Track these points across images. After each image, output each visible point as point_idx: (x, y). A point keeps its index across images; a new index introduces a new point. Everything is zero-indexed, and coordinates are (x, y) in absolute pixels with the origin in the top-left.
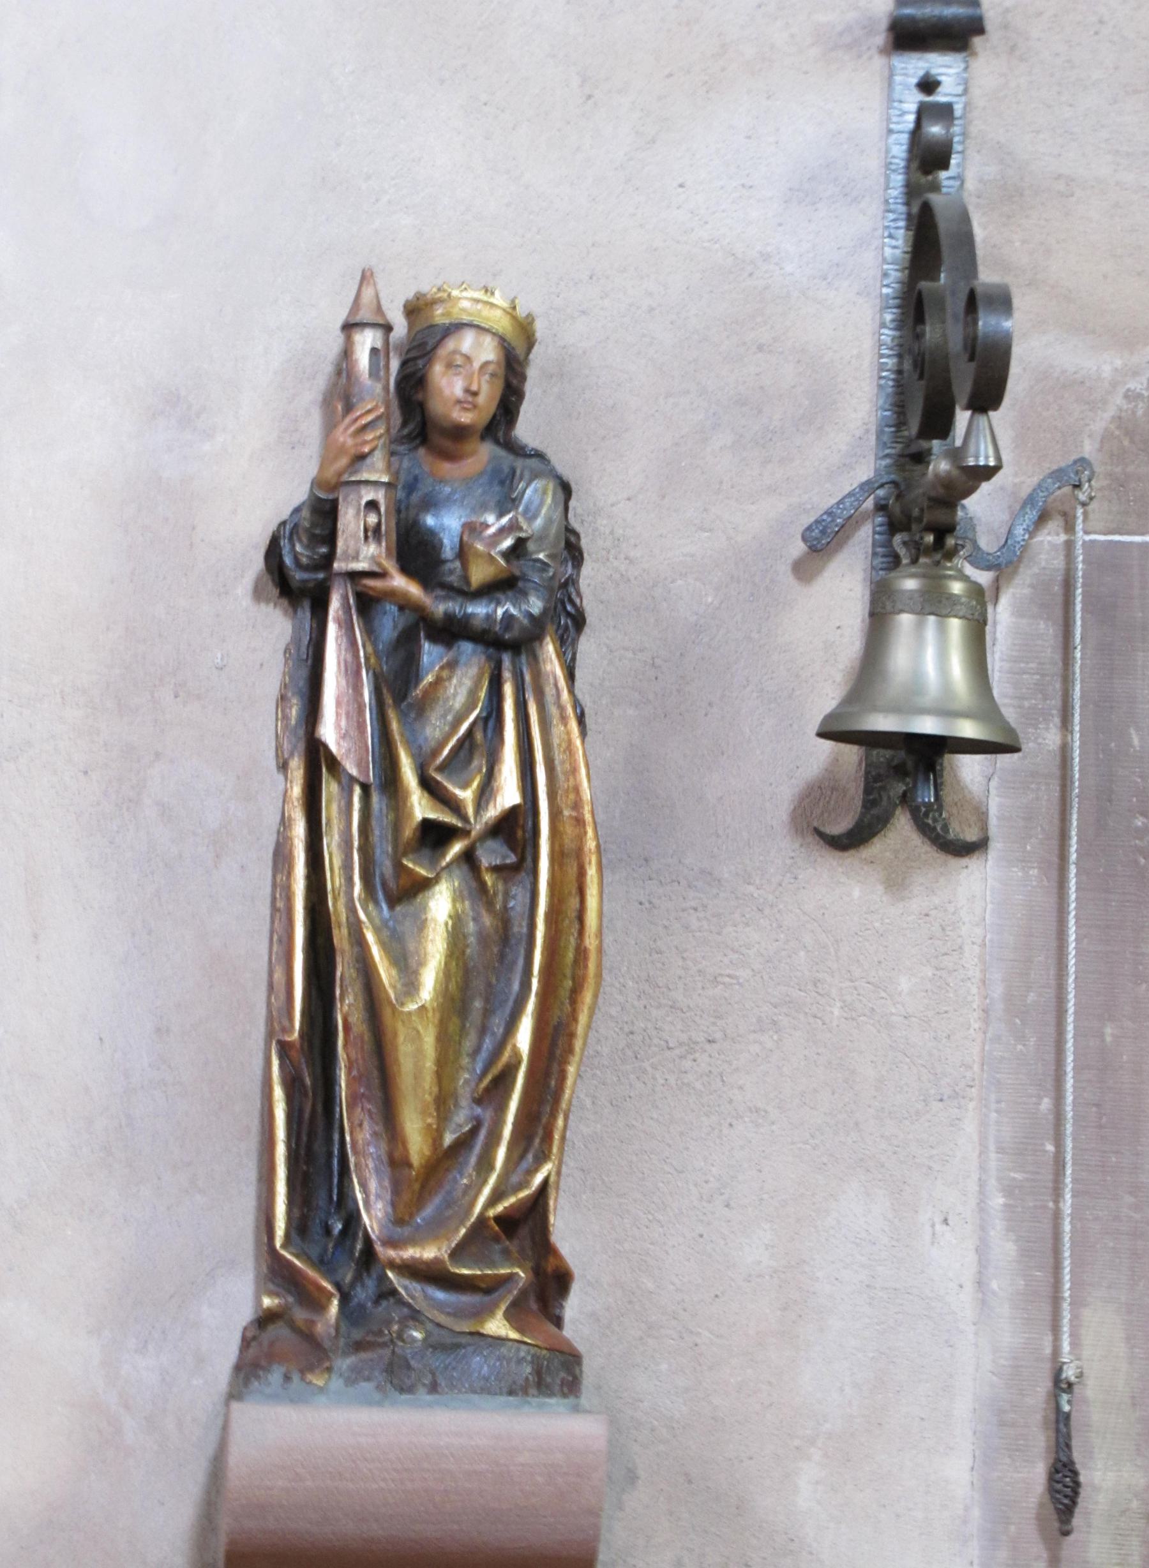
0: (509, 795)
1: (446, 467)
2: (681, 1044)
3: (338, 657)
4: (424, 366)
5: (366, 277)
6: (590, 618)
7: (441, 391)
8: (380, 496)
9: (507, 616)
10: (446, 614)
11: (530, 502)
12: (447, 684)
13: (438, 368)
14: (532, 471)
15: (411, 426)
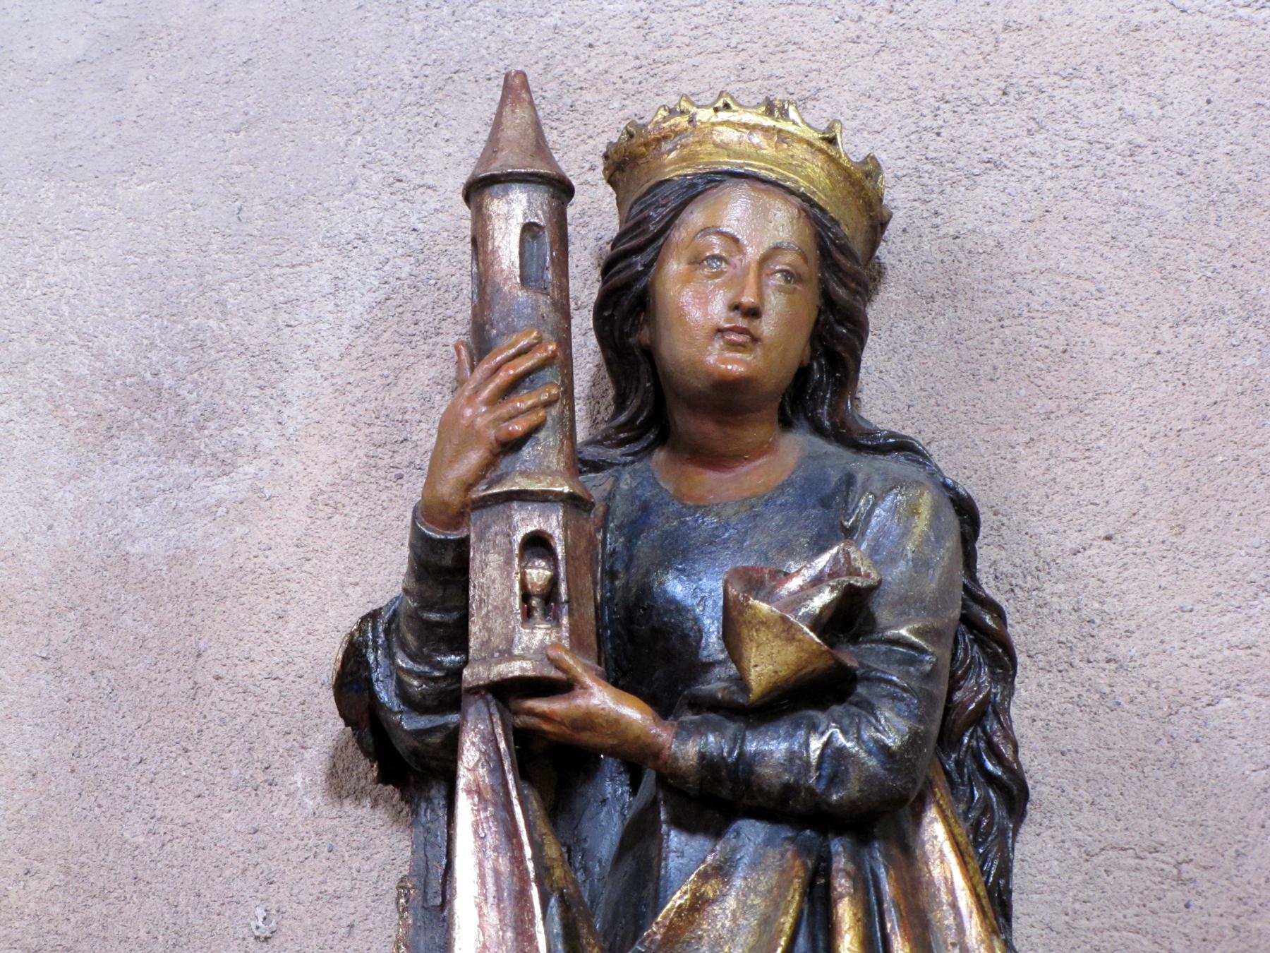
1: (709, 482)
3: (480, 864)
4: (648, 266)
5: (515, 88)
6: (1037, 791)
7: (682, 317)
8: (553, 523)
9: (833, 754)
10: (702, 756)
11: (883, 532)
12: (716, 909)
13: (674, 267)
14: (885, 476)
15: (633, 404)
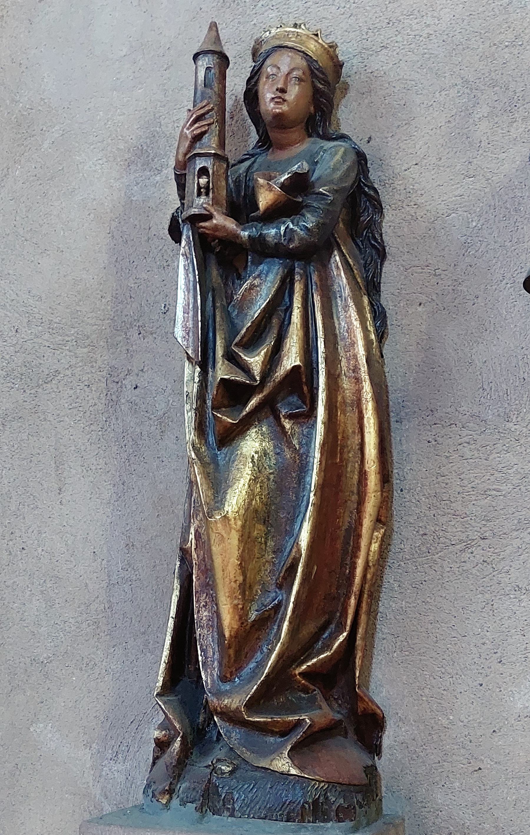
0: (292, 358)
2: (461, 541)
